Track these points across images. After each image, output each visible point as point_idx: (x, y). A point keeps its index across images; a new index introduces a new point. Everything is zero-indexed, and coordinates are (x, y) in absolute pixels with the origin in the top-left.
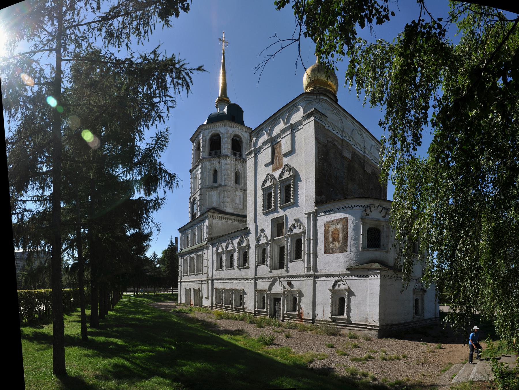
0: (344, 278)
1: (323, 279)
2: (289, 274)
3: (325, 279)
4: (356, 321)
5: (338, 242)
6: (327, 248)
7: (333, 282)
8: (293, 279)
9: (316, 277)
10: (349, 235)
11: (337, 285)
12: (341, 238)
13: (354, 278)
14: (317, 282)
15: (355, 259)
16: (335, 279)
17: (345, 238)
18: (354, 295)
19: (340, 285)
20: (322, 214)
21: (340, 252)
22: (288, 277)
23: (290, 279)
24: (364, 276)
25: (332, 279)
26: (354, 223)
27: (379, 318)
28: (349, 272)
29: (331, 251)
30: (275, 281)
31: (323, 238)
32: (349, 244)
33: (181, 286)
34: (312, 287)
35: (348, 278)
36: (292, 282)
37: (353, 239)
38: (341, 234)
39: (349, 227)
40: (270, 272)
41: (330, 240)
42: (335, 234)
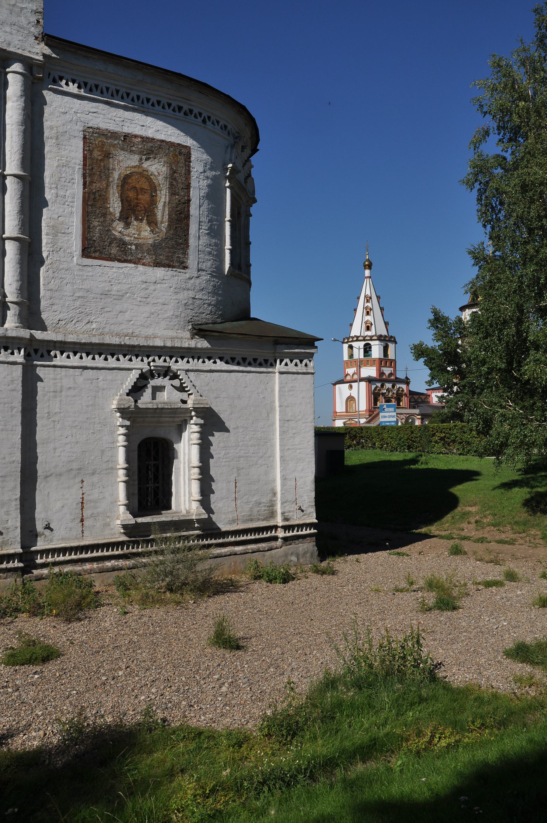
1: (75, 360)
3: (87, 361)
4: (233, 521)
5: (152, 223)
6: (96, 235)
7: (134, 376)
9: (38, 352)
10: (194, 210)
11: (148, 392)
12: (162, 212)
13: (221, 365)
14: (40, 372)
15: (213, 300)
16: (140, 365)
17: (180, 217)
18: (224, 429)
19: (161, 388)
20: (73, 88)
21: (157, 264)
24: (255, 362)
25: (124, 362)
26: (210, 174)
27: (316, 498)
28: (203, 344)
29: (114, 250)
31: (76, 190)
32: (192, 241)
33: (242, 372)
34: (18, 396)
35: (195, 364)
37: (205, 227)
38: (163, 197)
39: (194, 183)
41: (115, 206)
42: (139, 191)
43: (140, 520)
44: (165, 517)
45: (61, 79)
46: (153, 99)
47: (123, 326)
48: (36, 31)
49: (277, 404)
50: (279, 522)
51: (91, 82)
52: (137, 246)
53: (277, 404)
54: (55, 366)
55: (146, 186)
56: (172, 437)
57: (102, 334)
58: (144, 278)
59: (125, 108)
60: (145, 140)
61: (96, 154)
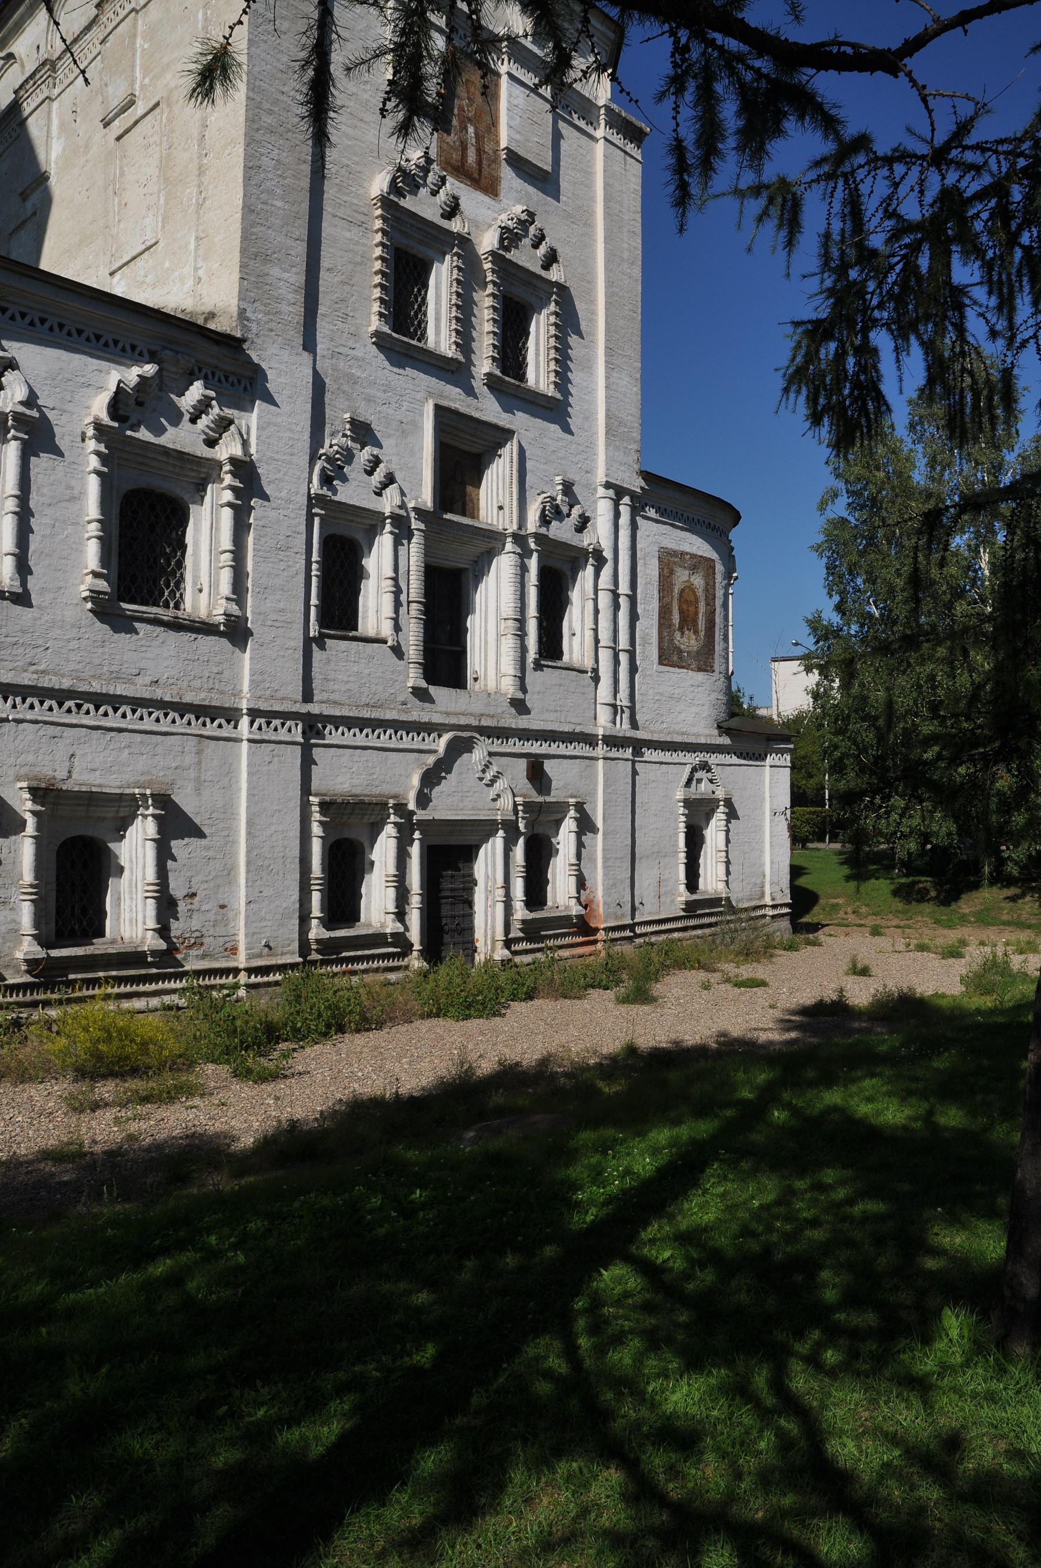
0: (713, 759)
2: (523, 722)
8: (554, 748)
13: (735, 760)
16: (694, 759)
22: (526, 735)
23: (536, 748)
28: (726, 741)
30: (459, 747)
31: (655, 605)
36: (549, 766)
40: (421, 695)
41: (676, 618)
43: (55, 953)
44: (98, 947)
45: (646, 505)
46: (108, 337)
47: (681, 726)
48: (636, 467)
49: (767, 795)
50: (768, 900)
51: (663, 507)
52: (688, 652)
53: (767, 795)
54: (645, 762)
55: (692, 599)
56: (703, 824)
57: (669, 733)
58: (691, 682)
59: (682, 529)
60: (693, 556)
61: (666, 571)
